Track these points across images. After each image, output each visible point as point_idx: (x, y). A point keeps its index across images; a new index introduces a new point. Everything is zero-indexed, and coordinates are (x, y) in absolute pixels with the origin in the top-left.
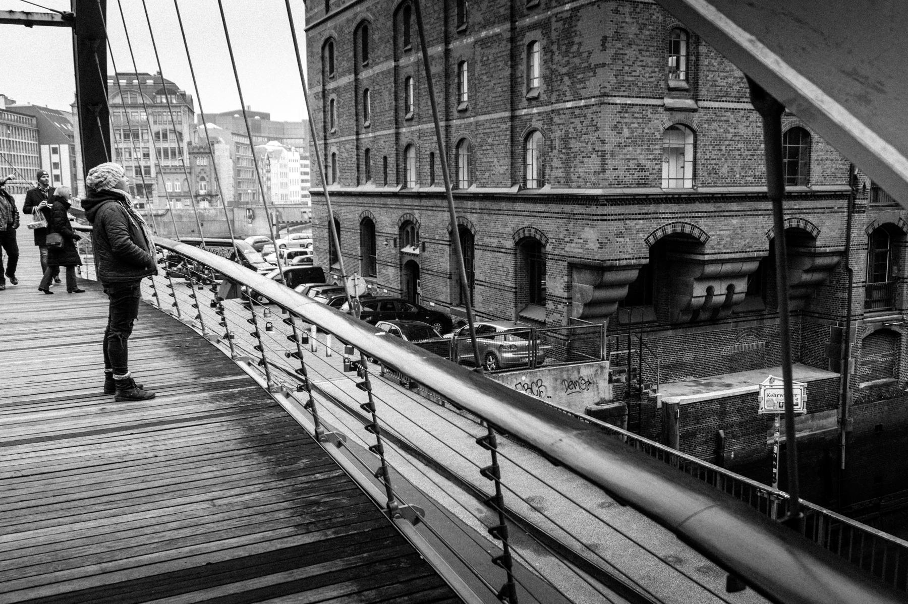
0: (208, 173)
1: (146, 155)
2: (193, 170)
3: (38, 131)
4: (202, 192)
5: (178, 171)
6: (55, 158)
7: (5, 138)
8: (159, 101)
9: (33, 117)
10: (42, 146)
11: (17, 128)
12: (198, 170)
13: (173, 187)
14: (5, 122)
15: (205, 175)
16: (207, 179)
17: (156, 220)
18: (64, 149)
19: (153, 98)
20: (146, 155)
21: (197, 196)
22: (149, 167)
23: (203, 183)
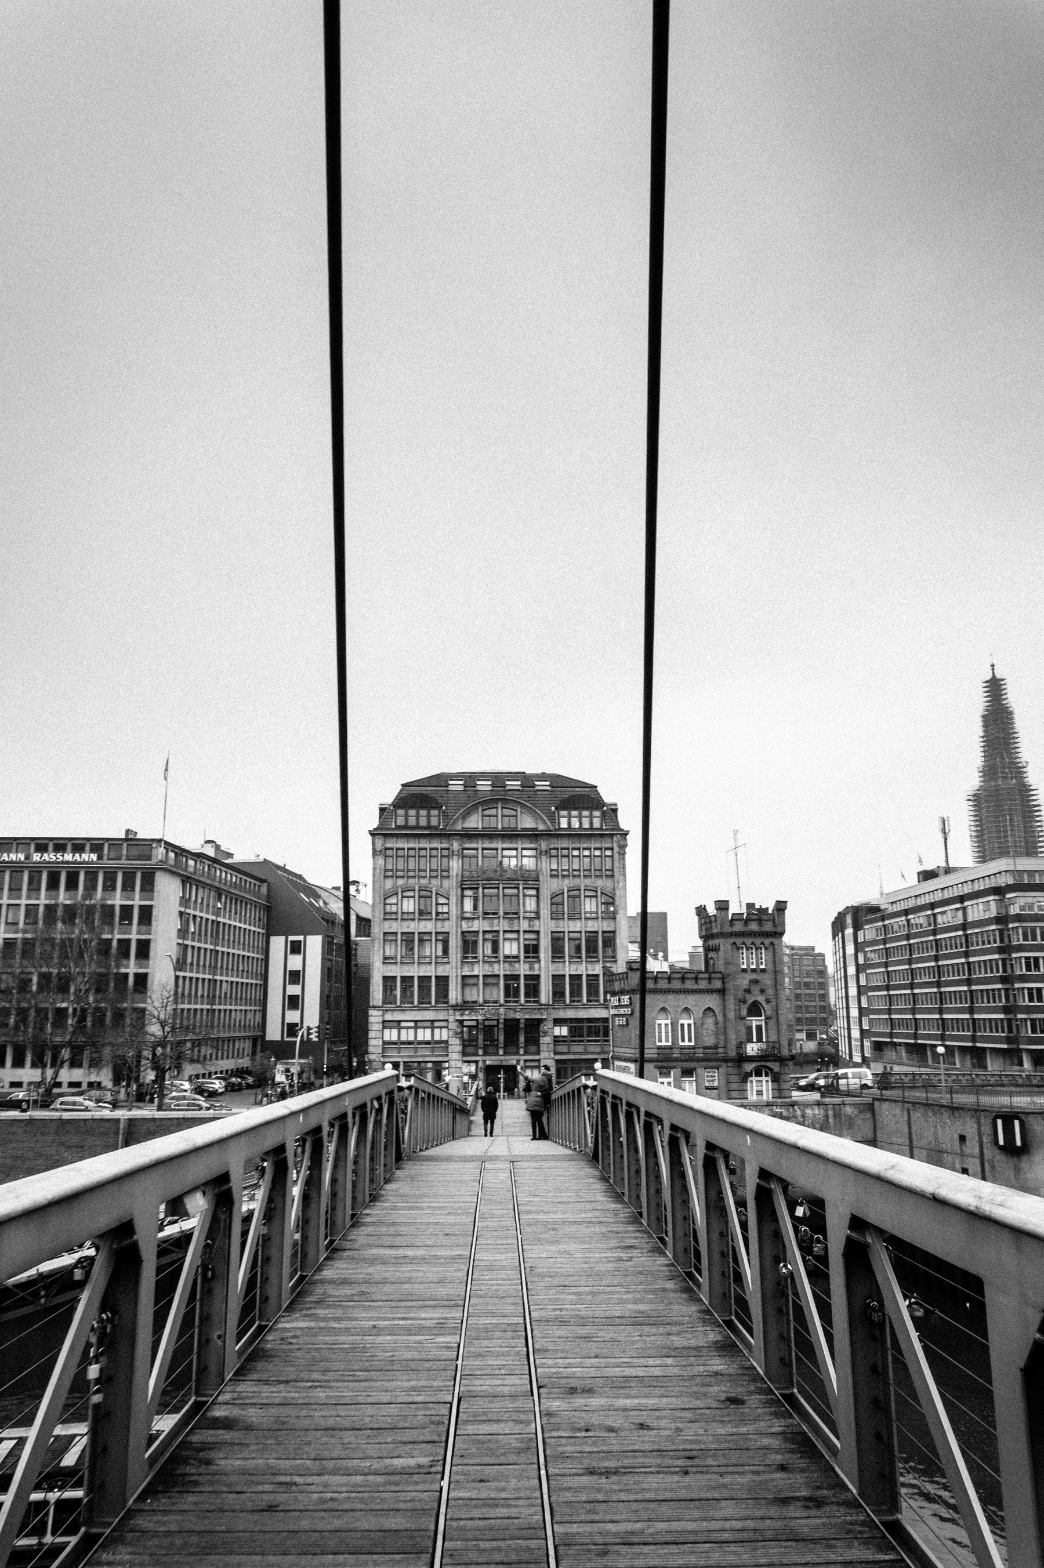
0: (770, 992)
1: (532, 951)
2: (730, 985)
3: (268, 907)
4: (752, 1049)
5: (689, 985)
6: (295, 962)
7: (211, 917)
8: (564, 824)
9: (262, 881)
10: (273, 939)
11: (237, 900)
12: (744, 981)
13: (674, 1031)
14: (216, 884)
15: (761, 999)
16: (768, 1009)
17: (249, 1037)
18: (314, 944)
19: (552, 817)
20: (532, 951)
21: (742, 1058)
22: (537, 977)
23: (755, 1022)
